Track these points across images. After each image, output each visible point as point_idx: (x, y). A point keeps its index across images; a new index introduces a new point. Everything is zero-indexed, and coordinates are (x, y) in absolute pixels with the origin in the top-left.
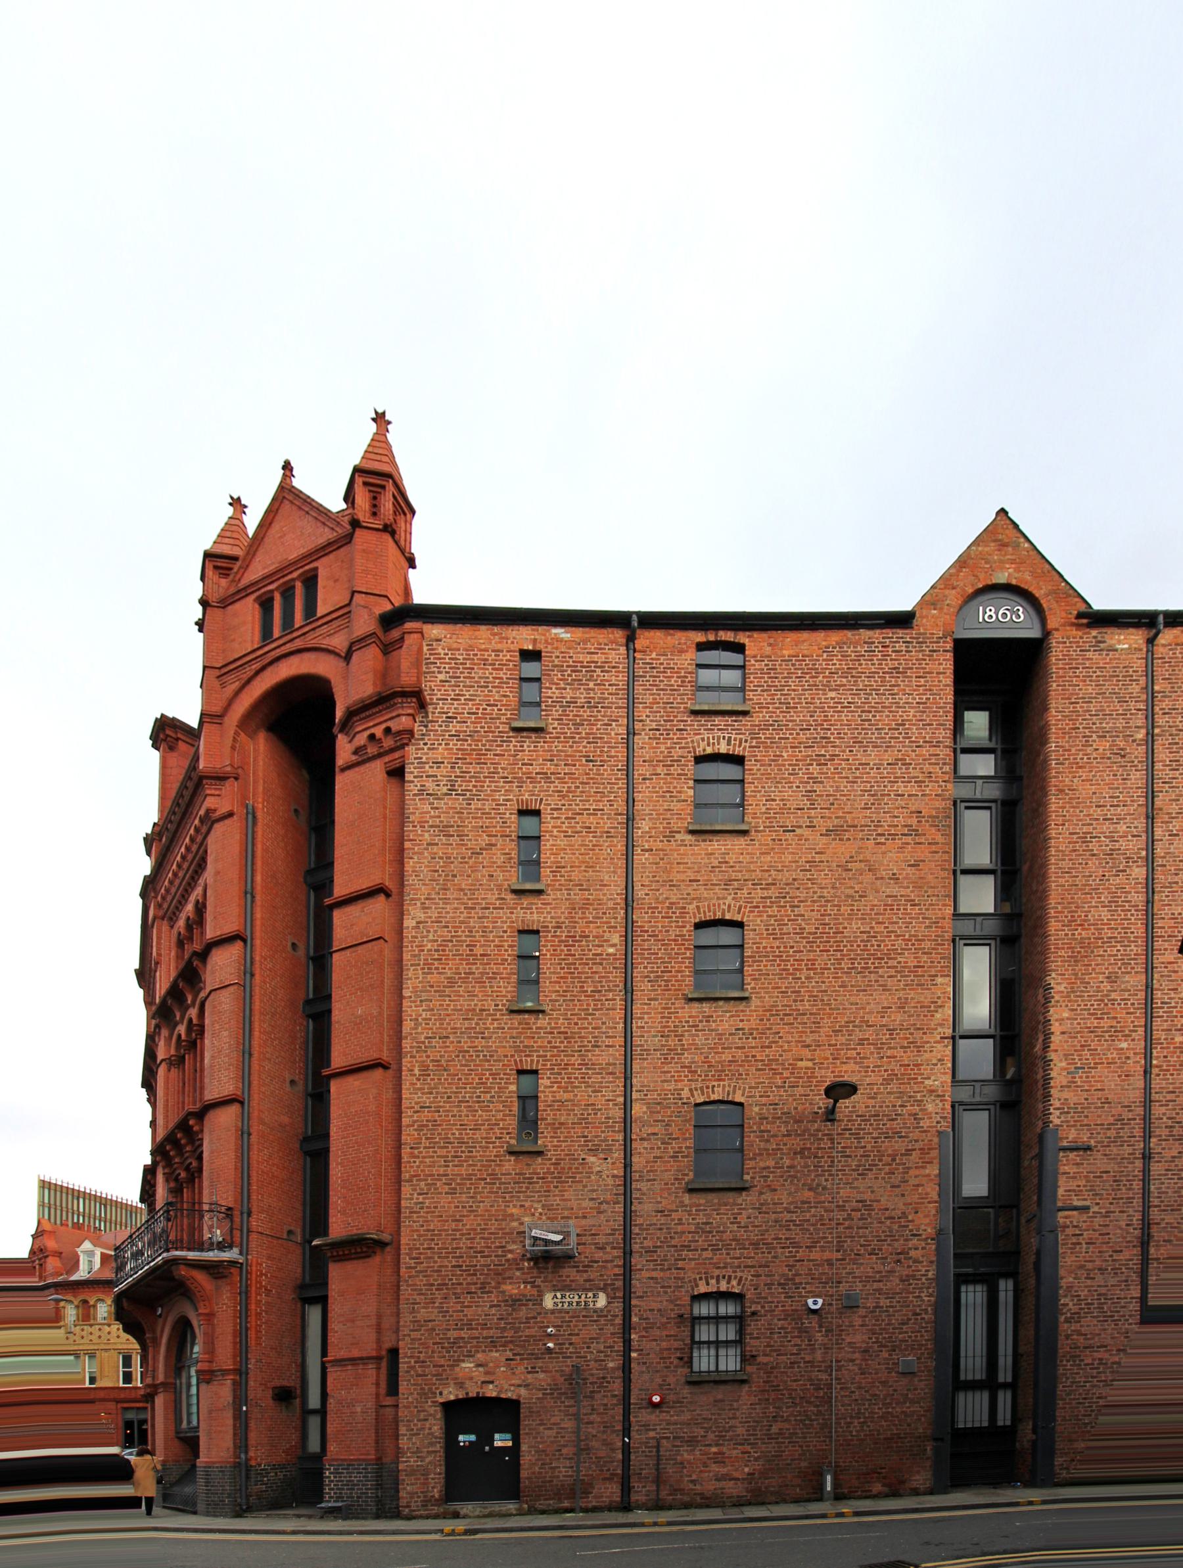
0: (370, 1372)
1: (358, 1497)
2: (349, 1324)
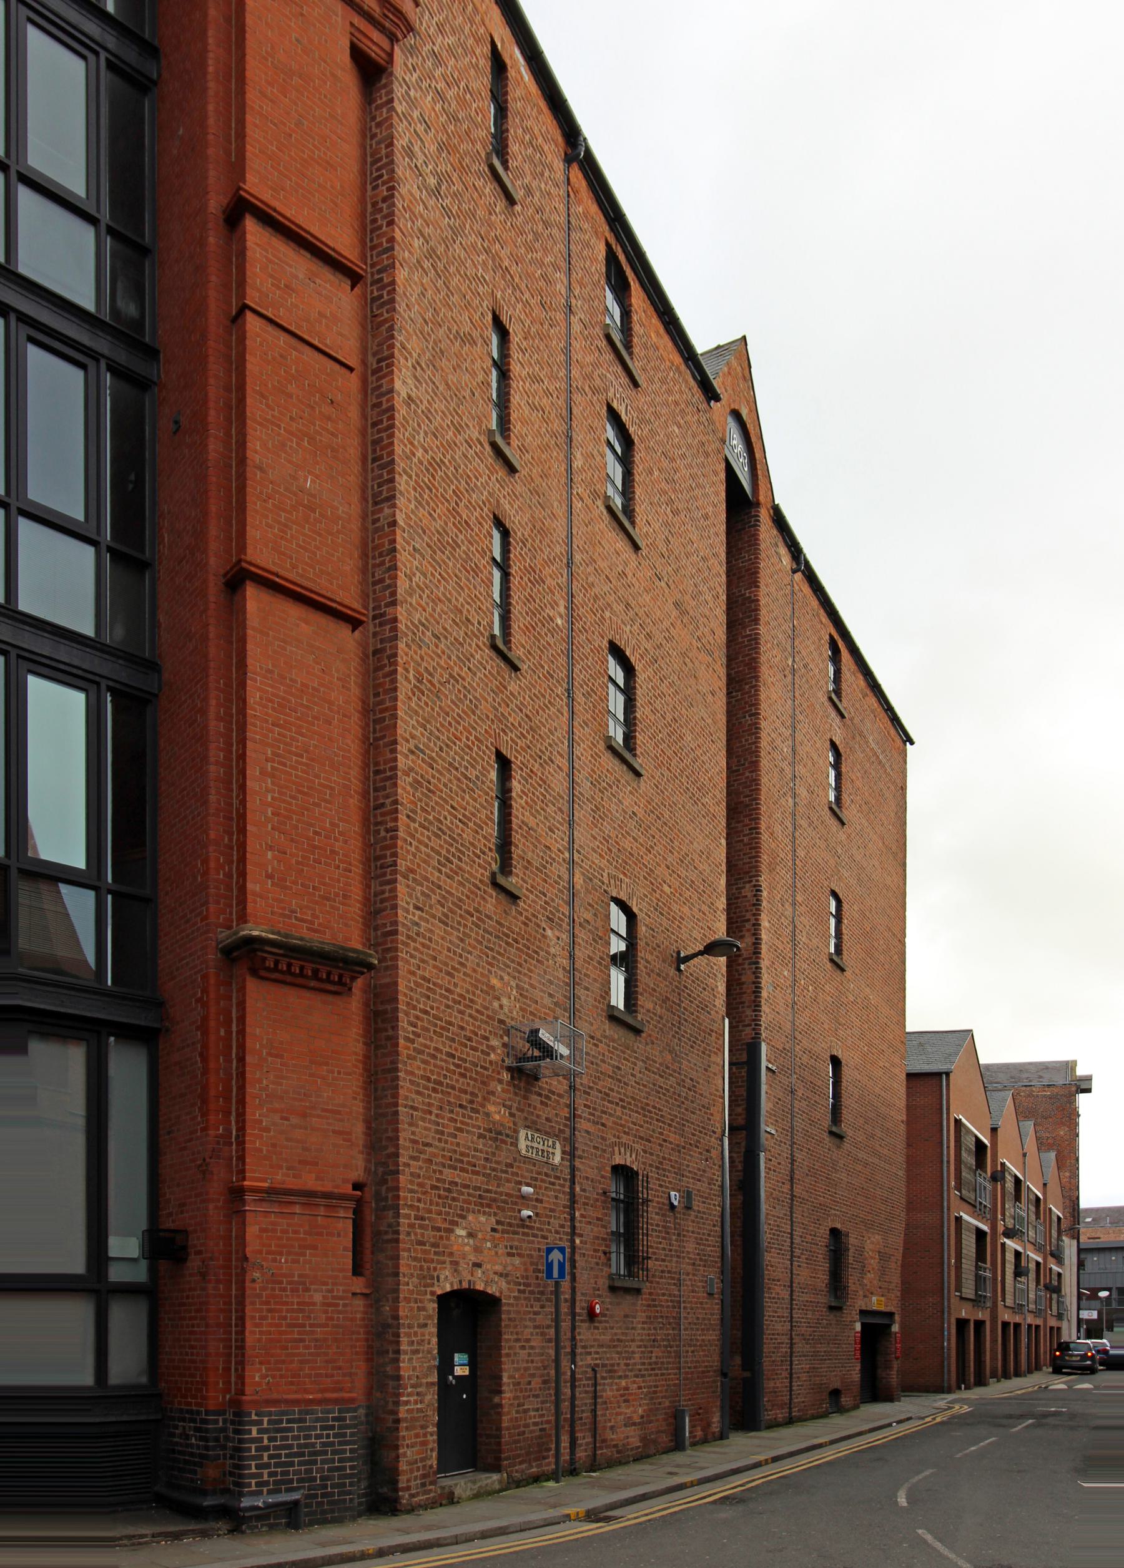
0: (340, 1225)
1: (322, 1478)
2: (294, 1120)
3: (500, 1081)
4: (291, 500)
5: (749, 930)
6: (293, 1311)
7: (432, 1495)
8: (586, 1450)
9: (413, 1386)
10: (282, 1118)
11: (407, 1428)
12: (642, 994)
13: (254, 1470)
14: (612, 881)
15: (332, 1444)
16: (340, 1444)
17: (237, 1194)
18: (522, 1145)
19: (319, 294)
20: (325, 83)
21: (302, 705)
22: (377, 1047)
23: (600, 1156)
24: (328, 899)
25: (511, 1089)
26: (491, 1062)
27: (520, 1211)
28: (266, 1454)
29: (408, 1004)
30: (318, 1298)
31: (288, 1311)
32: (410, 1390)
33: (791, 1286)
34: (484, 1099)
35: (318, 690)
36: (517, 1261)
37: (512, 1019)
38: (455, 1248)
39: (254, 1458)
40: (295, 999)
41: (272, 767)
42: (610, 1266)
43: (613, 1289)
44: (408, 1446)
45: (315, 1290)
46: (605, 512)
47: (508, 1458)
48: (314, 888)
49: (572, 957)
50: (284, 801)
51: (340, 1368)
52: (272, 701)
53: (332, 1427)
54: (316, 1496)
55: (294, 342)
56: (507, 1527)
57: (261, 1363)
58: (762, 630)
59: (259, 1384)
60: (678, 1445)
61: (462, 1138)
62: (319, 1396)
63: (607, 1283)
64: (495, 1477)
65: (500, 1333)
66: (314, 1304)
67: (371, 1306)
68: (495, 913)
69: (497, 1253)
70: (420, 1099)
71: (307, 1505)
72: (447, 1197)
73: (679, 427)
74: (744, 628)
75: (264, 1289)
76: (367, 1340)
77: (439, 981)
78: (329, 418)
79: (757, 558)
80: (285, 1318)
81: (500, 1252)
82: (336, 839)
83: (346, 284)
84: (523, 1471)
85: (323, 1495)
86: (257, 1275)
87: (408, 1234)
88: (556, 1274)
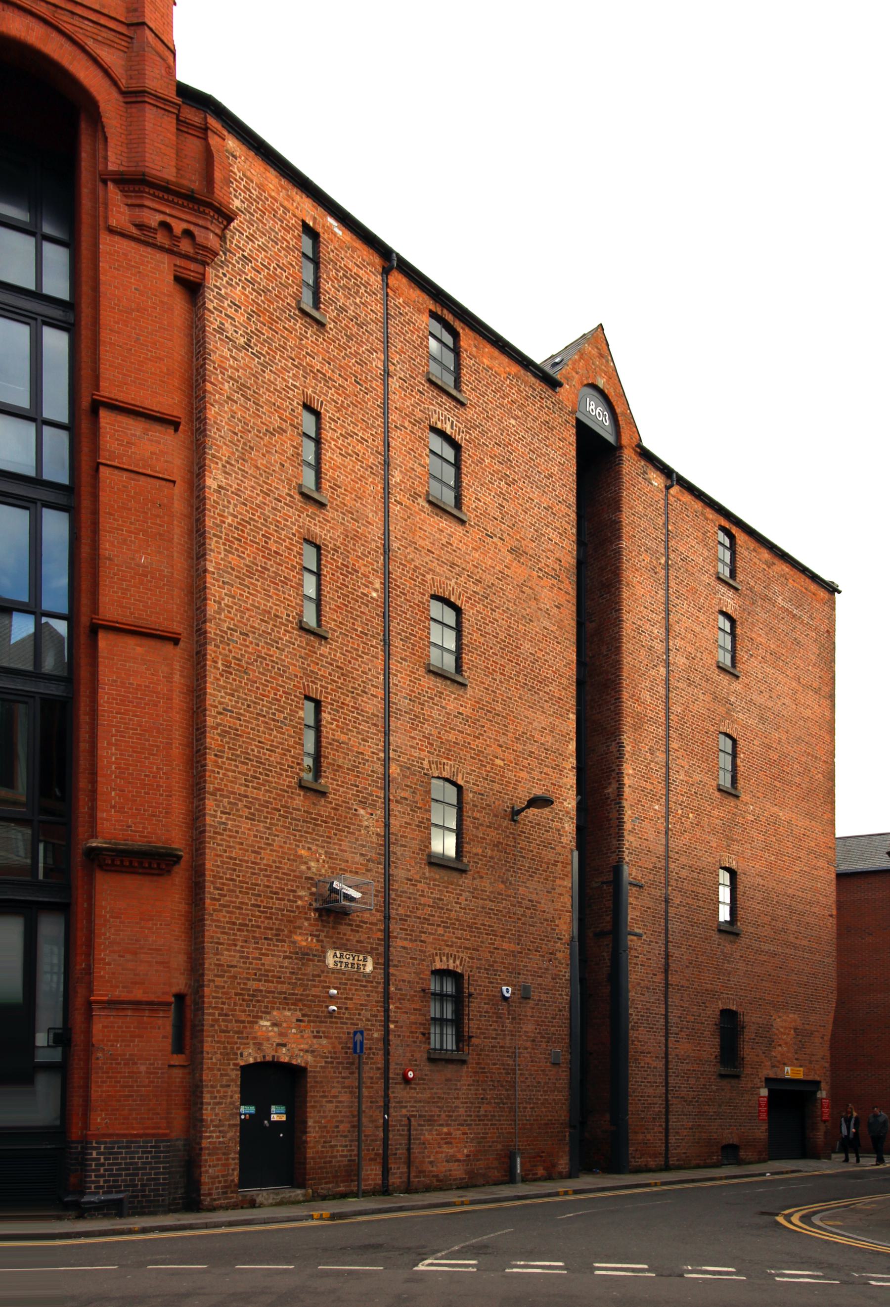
1: (142, 1185)
2: (128, 956)
3: (307, 919)
4: (130, 573)
5: (614, 778)
6: (125, 1077)
7: (233, 1200)
8: (401, 1178)
9: (215, 1126)
10: (120, 956)
11: (209, 1154)
12: (467, 843)
13: (93, 1178)
14: (433, 766)
15: (150, 1163)
16: (156, 1163)
17: (89, 1005)
18: (330, 961)
19: (152, 441)
20: (156, 308)
21: (137, 698)
22: (196, 906)
23: (419, 964)
24: (154, 816)
25: (320, 923)
26: (298, 907)
27: (327, 1007)
28: (102, 1168)
29: (214, 876)
30: (143, 1068)
31: (121, 1077)
32: (212, 1129)
33: (666, 1057)
34: (290, 932)
35: (148, 687)
36: (324, 1042)
37: (320, 875)
38: (259, 1034)
39: (94, 1171)
40: (129, 882)
41: (116, 740)
42: (429, 1043)
43: (431, 1060)
44: (210, 1166)
45: (141, 1064)
46: (426, 505)
47: (311, 1179)
48: (145, 810)
49: (387, 826)
50: (123, 759)
51: (158, 1114)
52: (116, 699)
53: (150, 1152)
54: (137, 1197)
55: (133, 475)
56: (253, 1219)
57: (102, 1111)
58: (624, 544)
59: (99, 1124)
60: (510, 1178)
61: (266, 960)
62: (142, 1131)
63: (425, 1056)
64: (299, 1192)
65: (306, 1092)
66: (140, 1073)
67: (189, 1074)
68: (303, 806)
69: (302, 1037)
70: (226, 937)
71: (130, 1202)
72: (252, 1001)
73: (516, 418)
74: (612, 544)
75: (104, 1064)
76: (185, 1096)
77: (246, 858)
78: (158, 516)
79: (620, 489)
80: (119, 1082)
81: (306, 1036)
82: (161, 778)
83: (171, 431)
84: (329, 1189)
85: (143, 1196)
86: (100, 1055)
87: (213, 1026)
88: (358, 1051)
